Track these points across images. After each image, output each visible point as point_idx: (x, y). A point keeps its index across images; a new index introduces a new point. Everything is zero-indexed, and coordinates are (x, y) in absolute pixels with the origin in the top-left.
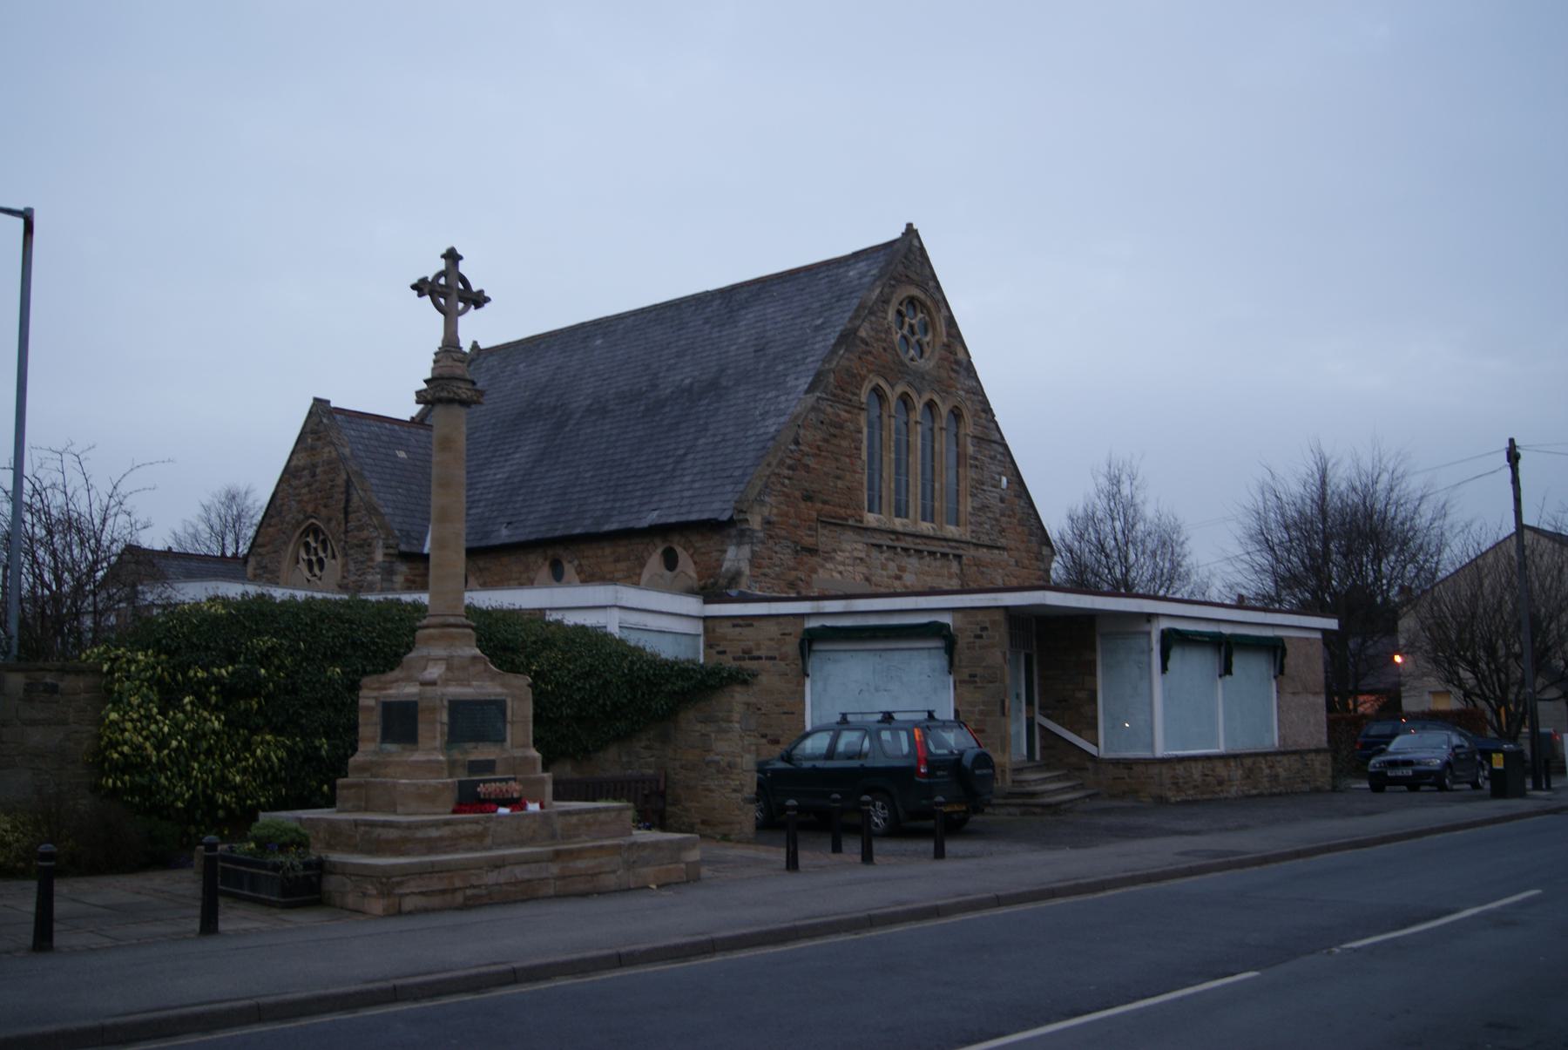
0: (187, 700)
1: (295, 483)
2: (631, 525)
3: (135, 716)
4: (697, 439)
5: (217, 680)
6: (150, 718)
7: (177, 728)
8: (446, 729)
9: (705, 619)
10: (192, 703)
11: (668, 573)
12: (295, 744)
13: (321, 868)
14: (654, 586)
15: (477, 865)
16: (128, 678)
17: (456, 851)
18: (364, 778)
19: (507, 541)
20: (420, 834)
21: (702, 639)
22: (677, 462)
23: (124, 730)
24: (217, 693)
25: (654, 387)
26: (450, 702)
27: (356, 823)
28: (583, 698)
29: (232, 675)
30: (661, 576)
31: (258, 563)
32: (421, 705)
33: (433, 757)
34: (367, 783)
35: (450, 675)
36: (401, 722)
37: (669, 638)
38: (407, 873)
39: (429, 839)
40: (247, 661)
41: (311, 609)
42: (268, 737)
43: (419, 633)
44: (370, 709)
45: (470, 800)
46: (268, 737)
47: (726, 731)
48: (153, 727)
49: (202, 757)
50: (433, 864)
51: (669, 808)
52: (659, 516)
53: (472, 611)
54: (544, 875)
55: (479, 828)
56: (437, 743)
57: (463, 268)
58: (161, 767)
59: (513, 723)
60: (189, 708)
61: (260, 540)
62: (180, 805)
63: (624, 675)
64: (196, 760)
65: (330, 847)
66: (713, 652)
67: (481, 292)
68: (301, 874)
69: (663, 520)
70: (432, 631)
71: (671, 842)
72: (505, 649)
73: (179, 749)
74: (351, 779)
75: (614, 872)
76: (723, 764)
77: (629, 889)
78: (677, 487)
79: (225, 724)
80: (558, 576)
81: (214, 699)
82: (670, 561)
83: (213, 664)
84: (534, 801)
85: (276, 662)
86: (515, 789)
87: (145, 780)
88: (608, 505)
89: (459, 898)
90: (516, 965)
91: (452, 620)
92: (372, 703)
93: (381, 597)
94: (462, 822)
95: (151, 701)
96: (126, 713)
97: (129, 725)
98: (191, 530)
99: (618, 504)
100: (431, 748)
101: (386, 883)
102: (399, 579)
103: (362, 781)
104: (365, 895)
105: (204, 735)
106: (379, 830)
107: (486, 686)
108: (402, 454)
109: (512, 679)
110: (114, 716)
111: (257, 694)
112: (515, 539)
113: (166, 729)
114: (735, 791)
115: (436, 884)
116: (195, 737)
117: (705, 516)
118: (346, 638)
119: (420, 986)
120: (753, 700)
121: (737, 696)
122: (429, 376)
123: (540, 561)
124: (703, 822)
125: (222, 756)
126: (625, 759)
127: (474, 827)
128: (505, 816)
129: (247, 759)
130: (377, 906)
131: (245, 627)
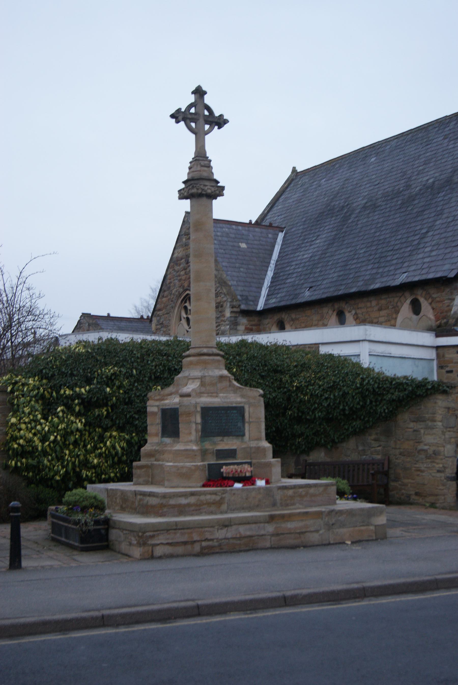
0: (59, 409)
1: (177, 268)
2: (388, 284)
3: (27, 420)
4: (435, 221)
5: (79, 396)
6: (36, 421)
7: (54, 427)
8: (200, 427)
9: (437, 348)
10: (63, 411)
11: (414, 317)
12: (132, 438)
13: (107, 523)
14: (404, 327)
15: (211, 525)
16: (23, 396)
17: (200, 514)
18: (151, 461)
19: (310, 299)
20: (172, 502)
21: (435, 363)
22: (421, 238)
23: (20, 430)
24: (79, 404)
25: (408, 187)
26: (202, 408)
27: (136, 493)
28: (329, 405)
29: (89, 391)
30: (410, 319)
31: (158, 321)
32: (180, 411)
33: (188, 447)
34: (152, 465)
35: (203, 389)
36: (171, 422)
37: (410, 362)
38: (158, 530)
39: (180, 506)
40: (98, 382)
41: (142, 348)
42: (114, 433)
43: (185, 361)
44: (154, 414)
45: (216, 478)
46: (114, 433)
47: (432, 428)
48: (39, 427)
49: (71, 447)
50: (176, 523)
51: (392, 484)
52: (407, 277)
53: (219, 345)
54: (262, 532)
55: (218, 498)
56: (193, 437)
57: (207, 100)
58: (45, 453)
59: (250, 423)
60: (61, 414)
61: (158, 306)
62: (58, 478)
63: (358, 388)
64: (68, 448)
65: (123, 509)
66: (444, 371)
67: (221, 116)
68: (92, 528)
69: (410, 280)
70: (191, 358)
71: (362, 510)
72: (276, 371)
73: (55, 441)
74: (143, 462)
75: (317, 531)
76: (430, 452)
77: (329, 544)
78: (421, 256)
79: (85, 425)
80: (342, 321)
81: (77, 409)
82: (416, 308)
83: (76, 385)
84: (262, 479)
85: (117, 383)
86: (247, 470)
87: (34, 462)
88: (374, 271)
89: (197, 548)
90: (200, 602)
91: (205, 351)
92: (155, 409)
93: (153, 337)
94: (205, 493)
95: (37, 410)
96: (21, 418)
97: (23, 426)
98: (145, 304)
99: (381, 270)
100: (190, 438)
101: (143, 536)
102: (241, 328)
103: (149, 463)
104: (130, 544)
105: (72, 432)
106: (148, 498)
107: (231, 396)
108: (243, 245)
109: (248, 391)
110: (13, 420)
111: (107, 405)
112: (314, 298)
113: (47, 429)
114: (439, 471)
115: (179, 537)
116: (66, 434)
117: (438, 275)
118: (164, 366)
119: (123, 616)
120: (452, 405)
121: (440, 403)
122: (186, 178)
123: (330, 312)
124: (417, 494)
125: (85, 446)
126: (361, 448)
127: (213, 497)
128: (238, 489)
129: (101, 448)
130: (137, 552)
131: (97, 360)
